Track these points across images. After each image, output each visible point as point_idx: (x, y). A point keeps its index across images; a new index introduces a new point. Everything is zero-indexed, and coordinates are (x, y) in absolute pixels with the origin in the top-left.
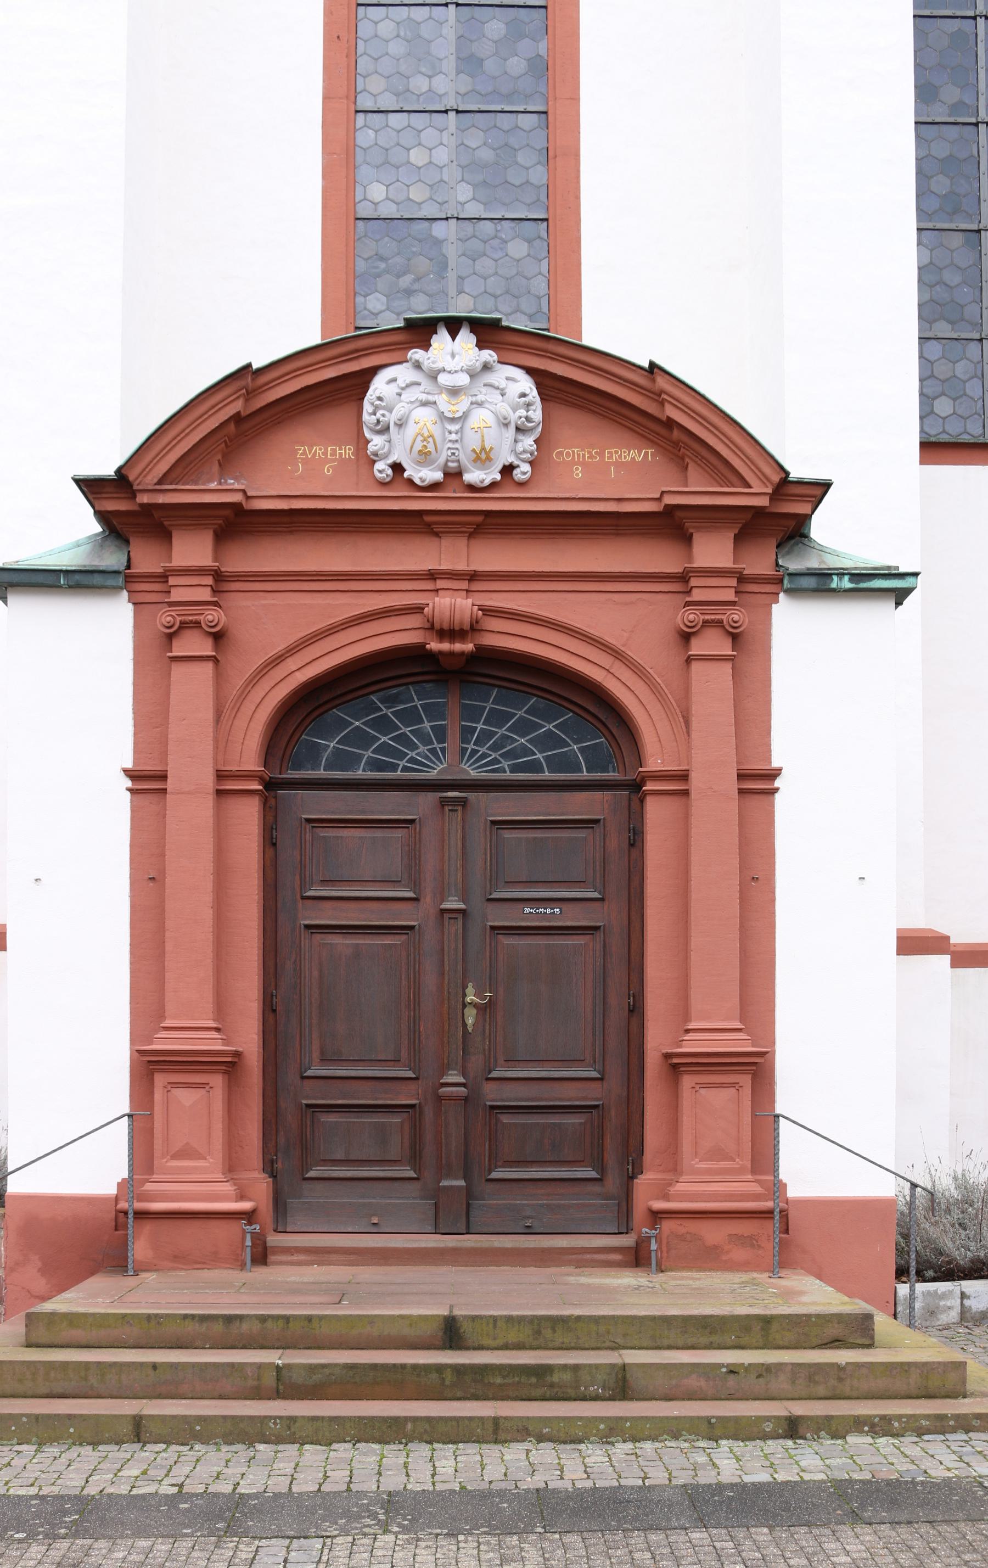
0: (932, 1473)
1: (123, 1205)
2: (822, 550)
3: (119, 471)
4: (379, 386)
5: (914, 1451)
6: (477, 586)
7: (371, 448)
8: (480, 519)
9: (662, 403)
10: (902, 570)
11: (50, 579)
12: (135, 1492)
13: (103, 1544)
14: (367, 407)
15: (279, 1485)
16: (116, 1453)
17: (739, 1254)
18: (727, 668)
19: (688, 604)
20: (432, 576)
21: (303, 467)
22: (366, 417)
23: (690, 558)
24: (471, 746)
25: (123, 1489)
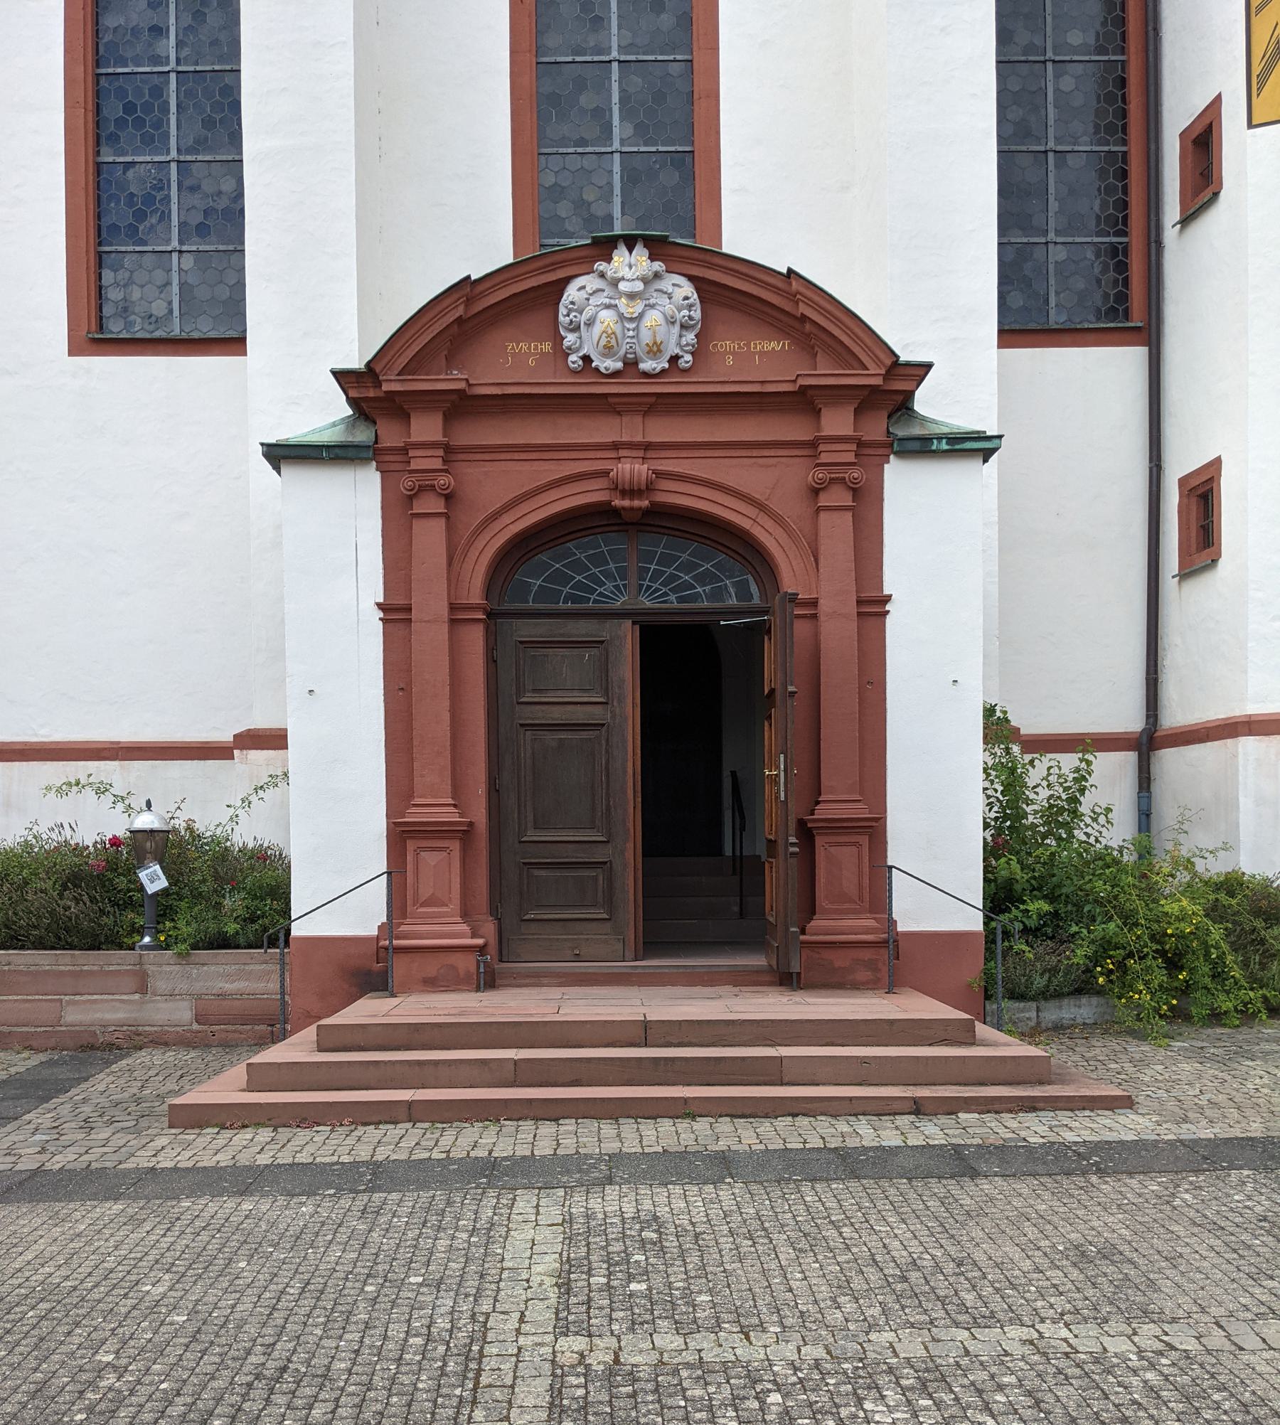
0: (1031, 1140)
1: (382, 943)
2: (924, 419)
3: (368, 364)
4: (572, 292)
5: (1013, 1124)
6: (650, 454)
7: (566, 343)
8: (653, 399)
9: (797, 303)
10: (988, 434)
11: (314, 453)
12: (413, 1157)
13: (395, 1196)
14: (563, 311)
15: (522, 1151)
16: (394, 1131)
17: (863, 975)
18: (849, 515)
19: (818, 465)
20: (616, 446)
21: (510, 361)
22: (561, 318)
23: (819, 429)
24: (647, 583)
25: (403, 1157)
